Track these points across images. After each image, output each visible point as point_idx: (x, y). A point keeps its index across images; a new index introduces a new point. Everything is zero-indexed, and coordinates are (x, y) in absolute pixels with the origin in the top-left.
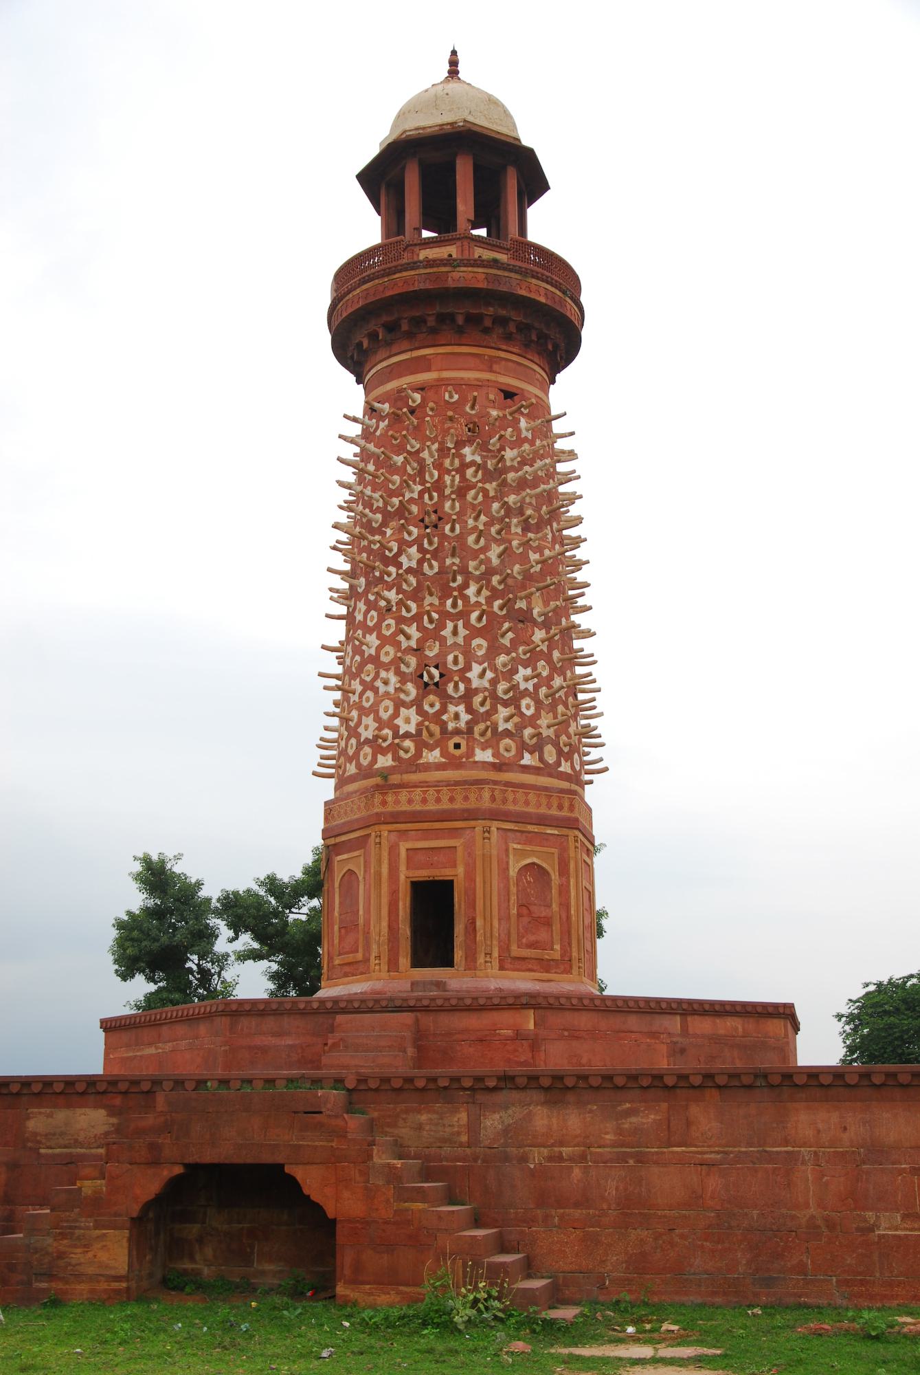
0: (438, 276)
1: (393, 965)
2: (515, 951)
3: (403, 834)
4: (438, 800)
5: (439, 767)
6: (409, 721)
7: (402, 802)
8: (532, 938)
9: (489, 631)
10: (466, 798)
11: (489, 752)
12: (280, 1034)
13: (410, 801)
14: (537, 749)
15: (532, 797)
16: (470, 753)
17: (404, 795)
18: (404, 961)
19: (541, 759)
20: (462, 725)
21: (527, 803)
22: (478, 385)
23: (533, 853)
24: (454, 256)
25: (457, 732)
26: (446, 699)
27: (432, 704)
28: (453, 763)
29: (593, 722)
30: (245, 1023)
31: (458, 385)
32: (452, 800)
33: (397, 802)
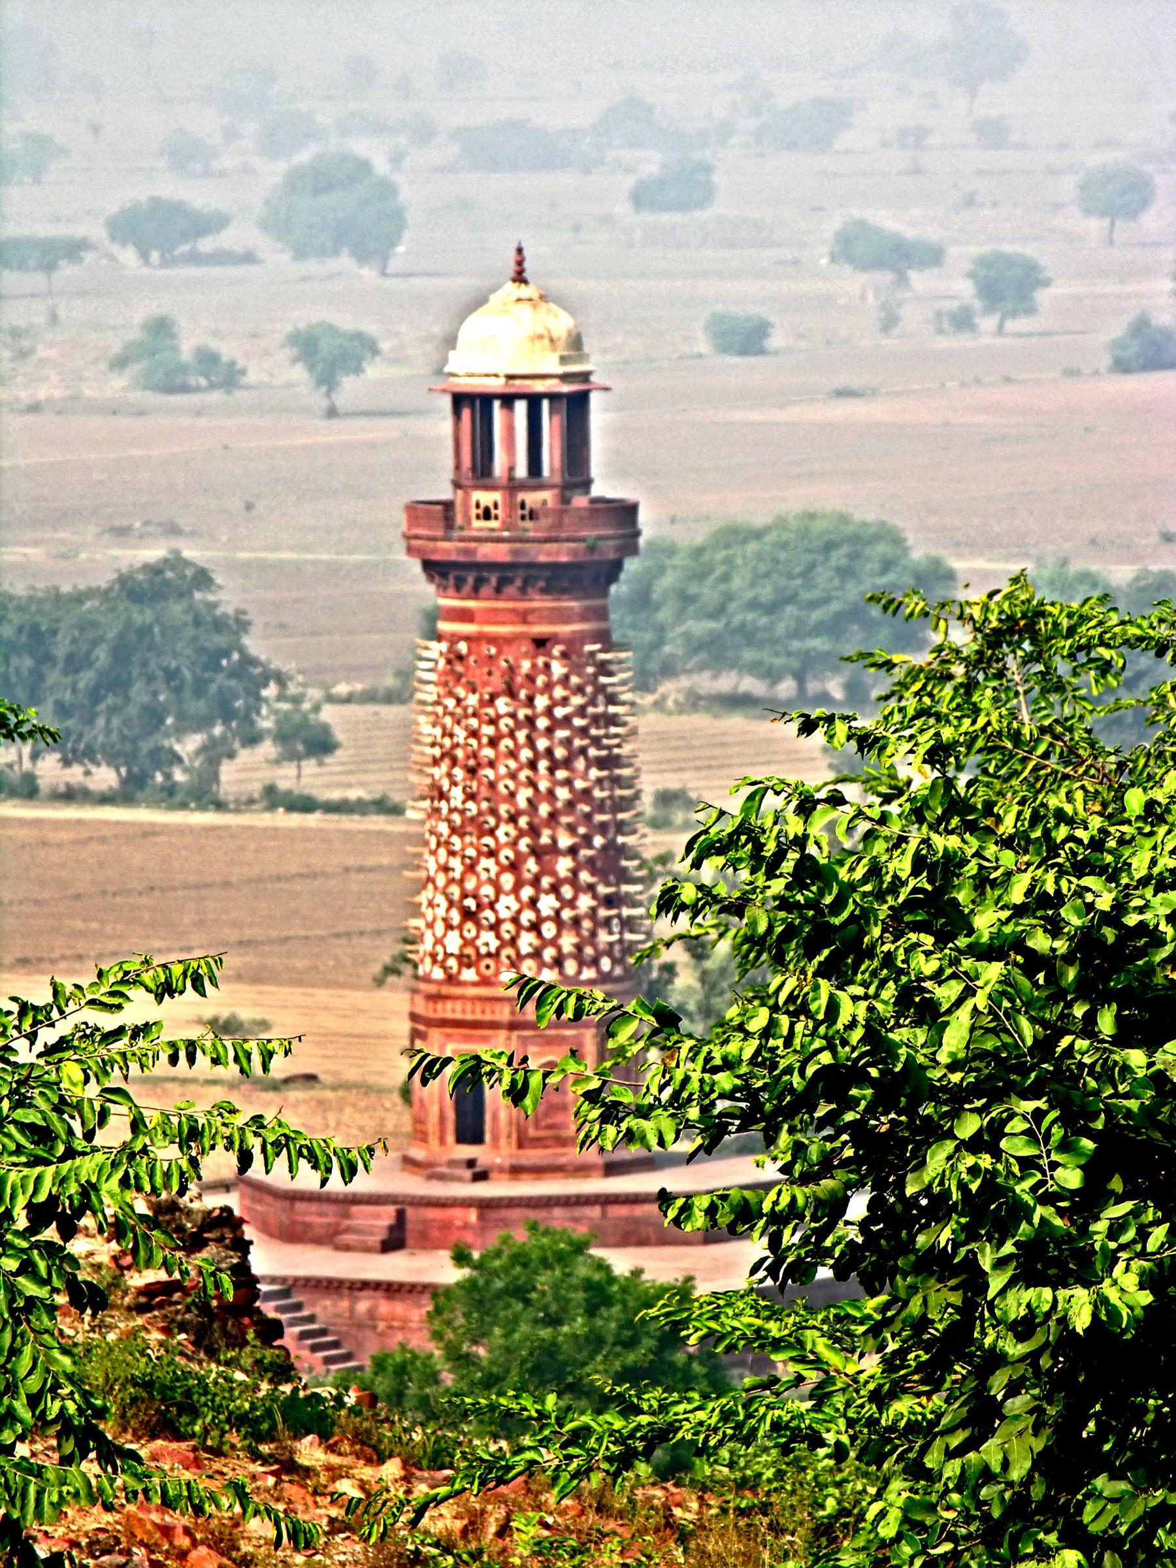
0: (466, 552)
1: (442, 1140)
2: (532, 1132)
3: (449, 1037)
4: (473, 1012)
5: (475, 984)
6: (453, 943)
7: (448, 1010)
8: (550, 1121)
9: (514, 867)
10: (483, 1012)
11: (473, 971)
12: (320, 1215)
13: (453, 1011)
14: (595, 962)
15: (469, 1006)
16: (497, 973)
17: (449, 1005)
18: (450, 1138)
19: (599, 971)
20: (493, 950)
21: (453, 1011)
22: (509, 640)
23: (550, 1053)
24: (550, 504)
25: (489, 955)
26: (479, 926)
27: (470, 929)
28: (485, 982)
29: (671, 915)
30: (300, 1206)
31: (492, 640)
32: (464, 1011)
33: (444, 1010)
